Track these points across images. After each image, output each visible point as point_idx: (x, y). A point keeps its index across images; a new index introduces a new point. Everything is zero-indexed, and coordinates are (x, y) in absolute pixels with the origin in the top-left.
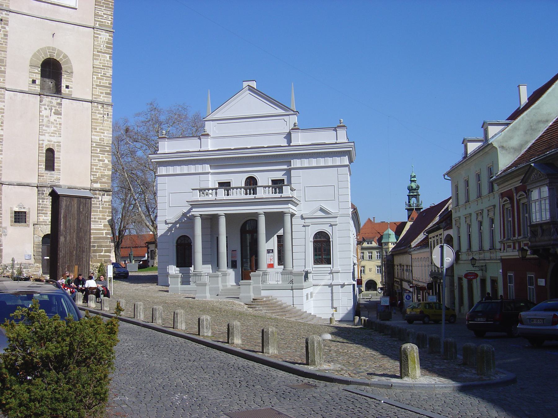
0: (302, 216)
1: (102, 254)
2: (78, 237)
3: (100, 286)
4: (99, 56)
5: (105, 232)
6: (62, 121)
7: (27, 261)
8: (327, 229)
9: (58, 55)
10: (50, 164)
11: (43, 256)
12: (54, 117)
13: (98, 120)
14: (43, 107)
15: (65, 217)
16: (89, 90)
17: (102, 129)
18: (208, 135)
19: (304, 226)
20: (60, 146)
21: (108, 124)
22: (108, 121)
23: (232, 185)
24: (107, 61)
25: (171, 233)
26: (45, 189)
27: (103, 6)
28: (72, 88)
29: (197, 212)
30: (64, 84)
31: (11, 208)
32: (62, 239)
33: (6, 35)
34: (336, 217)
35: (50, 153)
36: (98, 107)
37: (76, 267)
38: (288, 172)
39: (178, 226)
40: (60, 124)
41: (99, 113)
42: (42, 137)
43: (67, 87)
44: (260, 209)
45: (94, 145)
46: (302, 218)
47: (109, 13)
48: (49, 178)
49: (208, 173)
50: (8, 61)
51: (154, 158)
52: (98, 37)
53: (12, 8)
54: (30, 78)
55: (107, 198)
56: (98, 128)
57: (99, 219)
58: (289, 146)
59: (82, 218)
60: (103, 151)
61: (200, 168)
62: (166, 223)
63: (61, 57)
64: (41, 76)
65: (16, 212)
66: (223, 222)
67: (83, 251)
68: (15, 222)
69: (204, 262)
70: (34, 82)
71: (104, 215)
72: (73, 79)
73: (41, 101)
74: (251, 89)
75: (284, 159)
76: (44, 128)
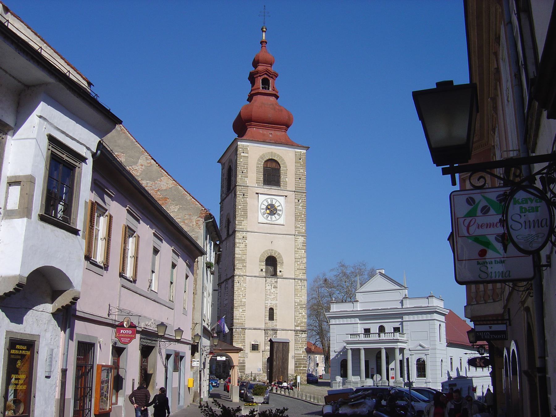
6: (278, 292)
8: (423, 357)
9: (275, 253)
12: (273, 290)
16: (293, 272)
18: (357, 301)
21: (305, 291)
29: (349, 347)
30: (278, 270)
32: (275, 363)
33: (246, 246)
35: (271, 310)
38: (402, 323)
42: (267, 302)
43: (280, 272)
44: (382, 346)
47: (303, 225)
50: (248, 260)
51: (327, 315)
53: (248, 230)
55: (304, 335)
59: (285, 353)
60: (302, 308)
61: (353, 320)
66: (363, 353)
69: (353, 375)
70: (262, 270)
73: (266, 281)
74: (381, 274)
75: (400, 315)
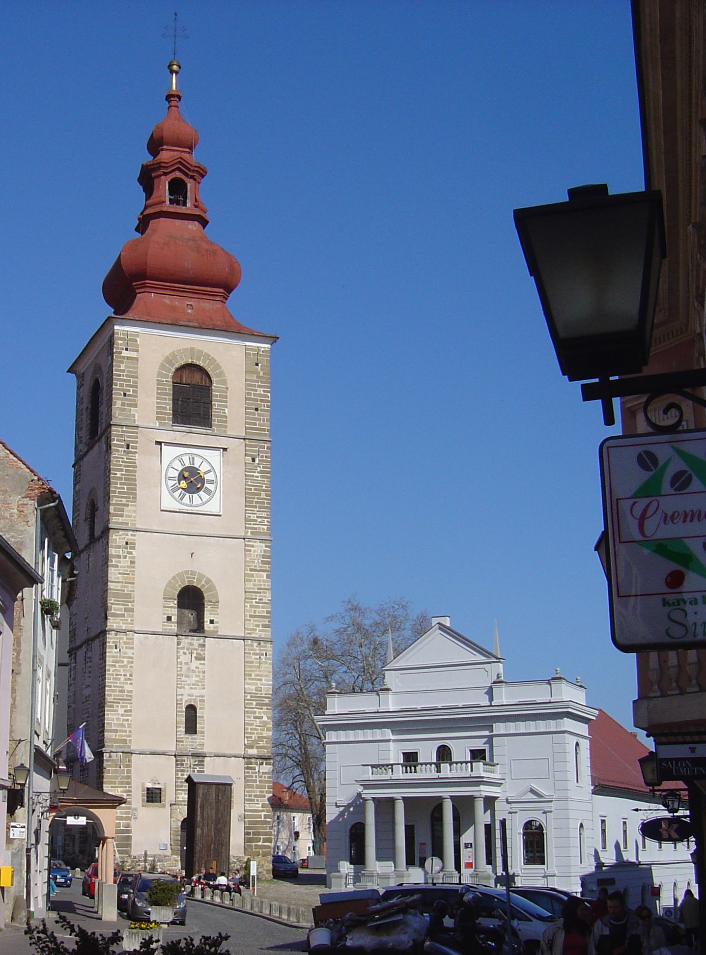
0: (507, 799)
1: (260, 844)
2: (216, 829)
3: (231, 883)
4: (252, 576)
5: (263, 813)
6: (205, 668)
7: (162, 853)
9: (199, 580)
10: (191, 726)
11: (182, 847)
12: (195, 664)
13: (252, 662)
14: (181, 651)
15: (202, 807)
17: (258, 675)
18: (388, 689)
19: (510, 813)
20: (204, 701)
21: (267, 668)
22: (266, 663)
23: (420, 760)
24: (264, 581)
25: (343, 818)
26: (185, 758)
27: (256, 507)
28: (217, 622)
29: (369, 794)
31: (143, 784)
32: (199, 831)
33: (132, 562)
34: (551, 801)
35: (191, 710)
36: (252, 646)
37: (215, 862)
38: (490, 740)
39: (351, 809)
40: (204, 672)
41: (254, 654)
42: (180, 691)
43: (212, 622)
45: (249, 697)
46: (508, 802)
48: (190, 743)
49: (389, 741)
52: (250, 551)
54: (164, 614)
55: (266, 768)
56: (253, 674)
57: (255, 796)
58: (491, 706)
60: (260, 705)
61: (378, 734)
62: (337, 806)
63: (203, 583)
64: (179, 607)
65: (148, 789)
66: (400, 807)
67: (222, 845)
68: (148, 801)
69: (379, 858)
70: (169, 619)
71: (262, 792)
72: (219, 611)
73: (178, 644)
75: (486, 723)
76: (183, 678)
